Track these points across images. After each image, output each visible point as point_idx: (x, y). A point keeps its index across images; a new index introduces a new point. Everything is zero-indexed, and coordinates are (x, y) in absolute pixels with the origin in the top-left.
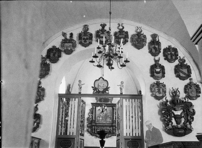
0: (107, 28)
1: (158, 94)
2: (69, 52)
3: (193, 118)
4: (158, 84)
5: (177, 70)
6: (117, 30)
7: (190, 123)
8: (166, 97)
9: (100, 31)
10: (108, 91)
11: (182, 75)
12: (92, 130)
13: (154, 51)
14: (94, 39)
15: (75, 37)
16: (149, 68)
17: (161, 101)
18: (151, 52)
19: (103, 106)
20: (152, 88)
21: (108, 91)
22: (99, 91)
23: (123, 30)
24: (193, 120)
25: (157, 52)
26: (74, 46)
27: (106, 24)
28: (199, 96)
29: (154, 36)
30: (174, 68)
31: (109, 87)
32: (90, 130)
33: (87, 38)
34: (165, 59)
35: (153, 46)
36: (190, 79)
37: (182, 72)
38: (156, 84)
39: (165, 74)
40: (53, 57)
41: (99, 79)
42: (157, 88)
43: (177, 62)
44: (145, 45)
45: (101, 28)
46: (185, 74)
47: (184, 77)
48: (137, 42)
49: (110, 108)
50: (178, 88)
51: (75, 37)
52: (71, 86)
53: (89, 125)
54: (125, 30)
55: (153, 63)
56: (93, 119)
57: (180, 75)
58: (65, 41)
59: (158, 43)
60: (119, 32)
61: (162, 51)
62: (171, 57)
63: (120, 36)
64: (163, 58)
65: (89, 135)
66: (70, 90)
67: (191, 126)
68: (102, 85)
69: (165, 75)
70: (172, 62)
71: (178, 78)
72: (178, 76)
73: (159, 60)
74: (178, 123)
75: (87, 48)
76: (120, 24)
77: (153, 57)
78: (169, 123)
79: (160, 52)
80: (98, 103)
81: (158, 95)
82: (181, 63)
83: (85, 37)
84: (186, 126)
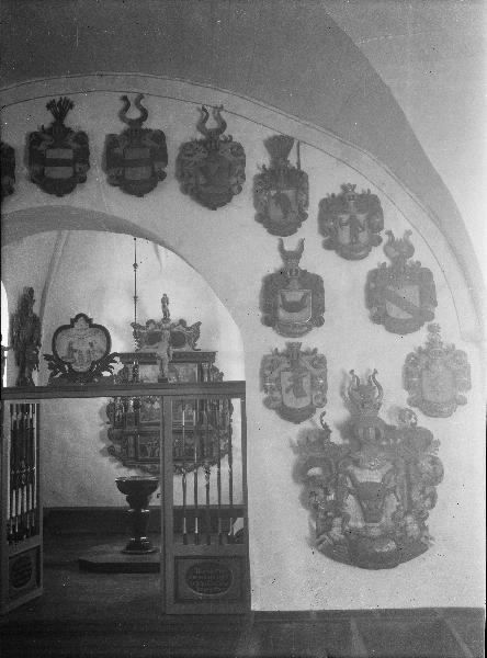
0: (76, 120)
3: (433, 497)
4: (293, 354)
6: (119, 127)
7: (421, 517)
8: (324, 414)
9: (46, 137)
11: (394, 311)
12: (127, 448)
13: (276, 213)
14: (22, 170)
16: (259, 285)
17: (306, 425)
18: (263, 218)
20: (267, 372)
22: (73, 374)
23: (146, 125)
24: (432, 506)
25: (292, 217)
27: (70, 97)
30: (363, 281)
34: (328, 246)
35: (273, 193)
37: (399, 301)
38: (287, 355)
39: (323, 310)
41: (73, 321)
42: (289, 374)
43: (377, 258)
44: (240, 189)
45: (47, 119)
48: (202, 180)
49: (191, 365)
50: (376, 372)
52: (37, 296)
54: (152, 124)
55: (274, 263)
56: (126, 409)
57: (386, 315)
59: (298, 179)
60: (125, 133)
61: (313, 210)
62: (354, 235)
63: (133, 154)
64: (320, 239)
65: (118, 467)
66: (36, 310)
67: (424, 528)
68: (85, 348)
69: (325, 316)
70: (362, 258)
71: (381, 328)
72: (379, 318)
73: (297, 255)
74: (369, 515)
76: (132, 98)
77: (275, 240)
78: (332, 518)
79: (304, 217)
80: (142, 351)
81: (291, 401)
82: (396, 261)
84: (404, 529)
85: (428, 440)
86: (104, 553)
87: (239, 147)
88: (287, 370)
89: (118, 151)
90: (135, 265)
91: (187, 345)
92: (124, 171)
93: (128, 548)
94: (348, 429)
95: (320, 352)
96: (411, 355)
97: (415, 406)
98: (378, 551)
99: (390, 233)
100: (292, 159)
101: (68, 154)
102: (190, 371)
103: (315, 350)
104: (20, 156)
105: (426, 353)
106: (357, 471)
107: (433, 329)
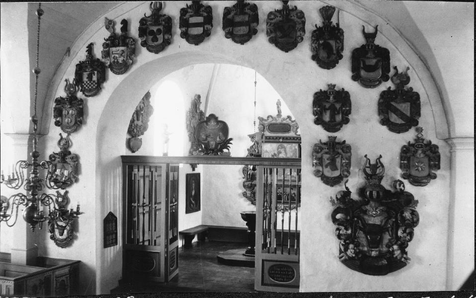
1: (328, 171)
2: (122, 68)
3: (411, 234)
5: (386, 105)
7: (403, 247)
8: (347, 181)
9: (189, 10)
10: (227, 147)
11: (394, 118)
13: (323, 54)
14: (177, 30)
15: (134, 31)
19: (69, 285)
21: (228, 150)
24: (410, 240)
26: (133, 52)
28: (435, 177)
29: (327, 12)
31: (231, 139)
32: (249, 193)
33: (159, 30)
36: (417, 130)
37: (396, 111)
40: (88, 82)
42: (328, 156)
44: (302, 39)
46: (401, 115)
47: (401, 125)
49: (294, 145)
51: (134, 31)
52: (203, 100)
53: (248, 183)
58: (113, 41)
65: (248, 205)
67: (404, 252)
72: (385, 122)
75: (161, 55)
79: (341, 57)
81: (328, 173)
82: (397, 86)
83: (155, 29)
85: (410, 200)
86: (233, 254)
87: (302, 13)
88: (326, 153)
89: (230, 17)
90: (255, 83)
91: (292, 132)
92: (232, 29)
93: (246, 252)
94: (362, 191)
95: (347, 142)
96: (404, 146)
97: (405, 178)
98: (376, 264)
99: (395, 68)
100: (334, 20)
101: (200, 19)
102: (293, 148)
103: (345, 141)
104: (177, 21)
105: (413, 145)
106: (366, 217)
107: (419, 130)
